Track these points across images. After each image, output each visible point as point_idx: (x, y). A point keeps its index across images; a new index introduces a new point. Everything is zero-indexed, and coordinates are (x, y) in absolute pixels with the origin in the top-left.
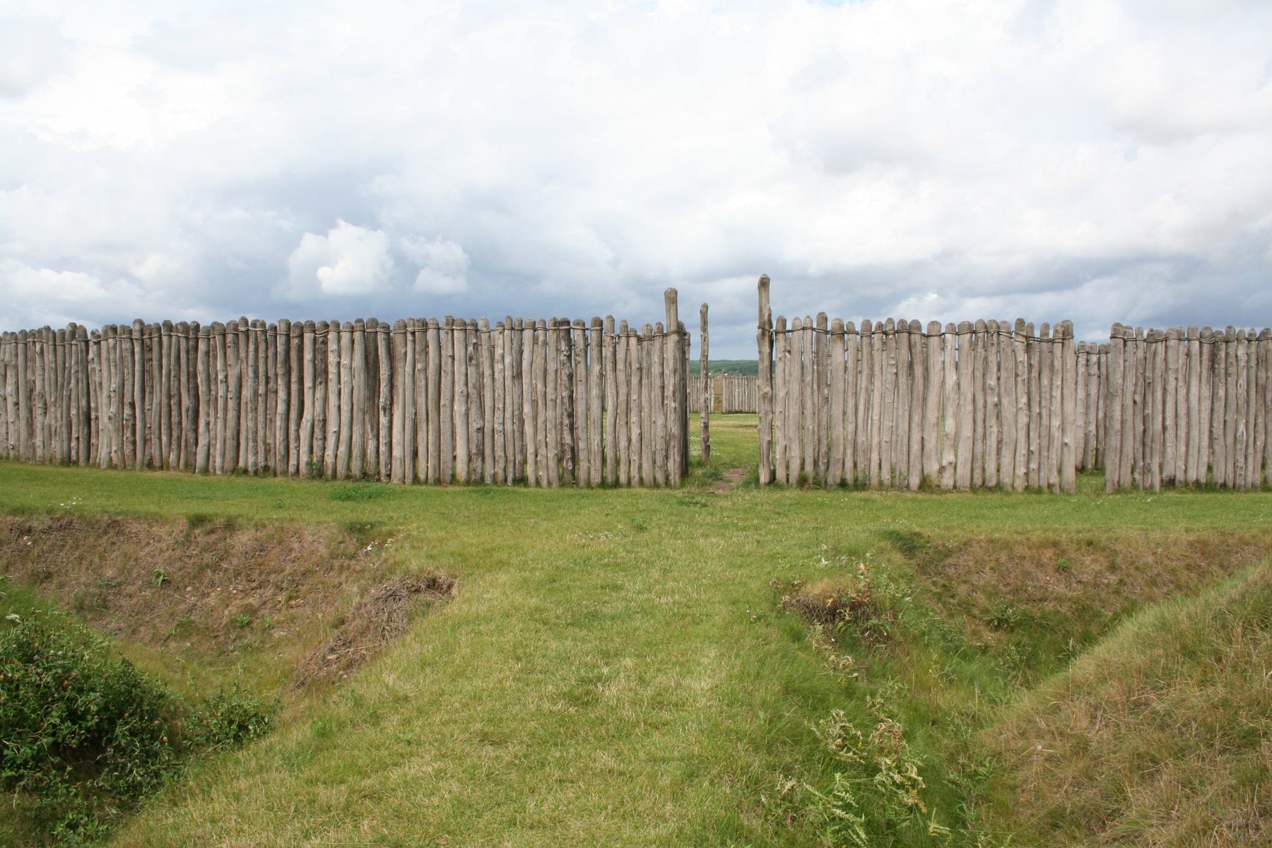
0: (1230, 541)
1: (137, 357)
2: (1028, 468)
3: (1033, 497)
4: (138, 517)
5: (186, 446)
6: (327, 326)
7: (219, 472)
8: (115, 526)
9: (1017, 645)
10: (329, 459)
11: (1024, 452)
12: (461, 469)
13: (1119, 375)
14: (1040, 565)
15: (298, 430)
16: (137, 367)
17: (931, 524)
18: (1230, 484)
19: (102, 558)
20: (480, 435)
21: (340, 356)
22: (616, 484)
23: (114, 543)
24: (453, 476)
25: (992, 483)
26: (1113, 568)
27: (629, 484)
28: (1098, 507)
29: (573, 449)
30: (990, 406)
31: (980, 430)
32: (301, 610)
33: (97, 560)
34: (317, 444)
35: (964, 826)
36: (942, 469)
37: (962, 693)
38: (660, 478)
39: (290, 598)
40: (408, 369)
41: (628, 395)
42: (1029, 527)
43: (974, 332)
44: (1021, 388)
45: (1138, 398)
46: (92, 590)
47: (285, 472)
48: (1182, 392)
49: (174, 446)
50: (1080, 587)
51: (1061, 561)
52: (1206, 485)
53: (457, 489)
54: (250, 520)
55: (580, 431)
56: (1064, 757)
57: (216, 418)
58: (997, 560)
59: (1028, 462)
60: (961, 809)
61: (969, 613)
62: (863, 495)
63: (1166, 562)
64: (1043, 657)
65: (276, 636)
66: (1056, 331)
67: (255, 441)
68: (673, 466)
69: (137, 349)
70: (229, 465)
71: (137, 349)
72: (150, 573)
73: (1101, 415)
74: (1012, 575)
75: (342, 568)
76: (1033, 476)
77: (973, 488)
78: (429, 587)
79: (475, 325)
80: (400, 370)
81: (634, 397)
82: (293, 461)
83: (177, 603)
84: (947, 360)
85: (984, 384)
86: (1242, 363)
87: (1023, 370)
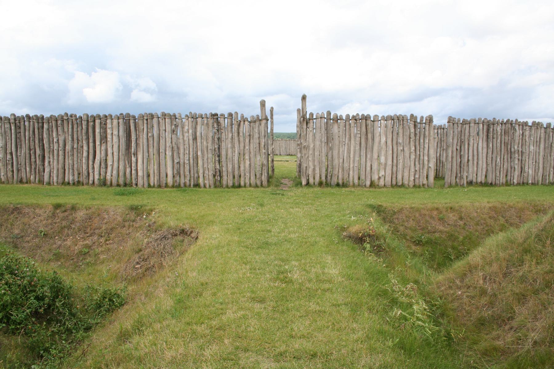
0: (506, 207)
1: (13, 131)
3: (418, 189)
4: (28, 206)
5: (39, 173)
6: (106, 116)
7: (55, 184)
8: (17, 210)
10: (108, 177)
12: (170, 180)
13: (451, 138)
14: (431, 217)
15: (93, 164)
16: (13, 136)
18: (494, 183)
19: (12, 225)
20: (178, 165)
21: (112, 131)
22: (239, 186)
23: (17, 218)
24: (166, 184)
25: (400, 184)
26: (461, 218)
27: (245, 186)
29: (220, 171)
30: (399, 151)
31: (395, 161)
32: (112, 246)
33: (9, 226)
34: (103, 171)
36: (379, 178)
38: (259, 183)
39: (106, 240)
40: (145, 136)
41: (244, 147)
44: (412, 143)
45: (458, 148)
46: (9, 240)
47: (88, 184)
49: (33, 173)
50: (448, 226)
53: (168, 189)
54: (83, 205)
55: (223, 163)
57: (53, 159)
58: (415, 216)
59: (415, 175)
61: (405, 239)
62: (347, 189)
63: (482, 215)
65: (101, 258)
66: (426, 119)
67: (73, 170)
68: (264, 178)
69: (13, 128)
70: (60, 180)
71: (13, 128)
72: (36, 231)
74: (421, 222)
75: (129, 226)
76: (417, 181)
77: (392, 186)
78: (181, 233)
79: (175, 115)
80: (141, 136)
81: (247, 147)
82: (91, 178)
83: (52, 245)
85: (397, 142)
86: (499, 133)
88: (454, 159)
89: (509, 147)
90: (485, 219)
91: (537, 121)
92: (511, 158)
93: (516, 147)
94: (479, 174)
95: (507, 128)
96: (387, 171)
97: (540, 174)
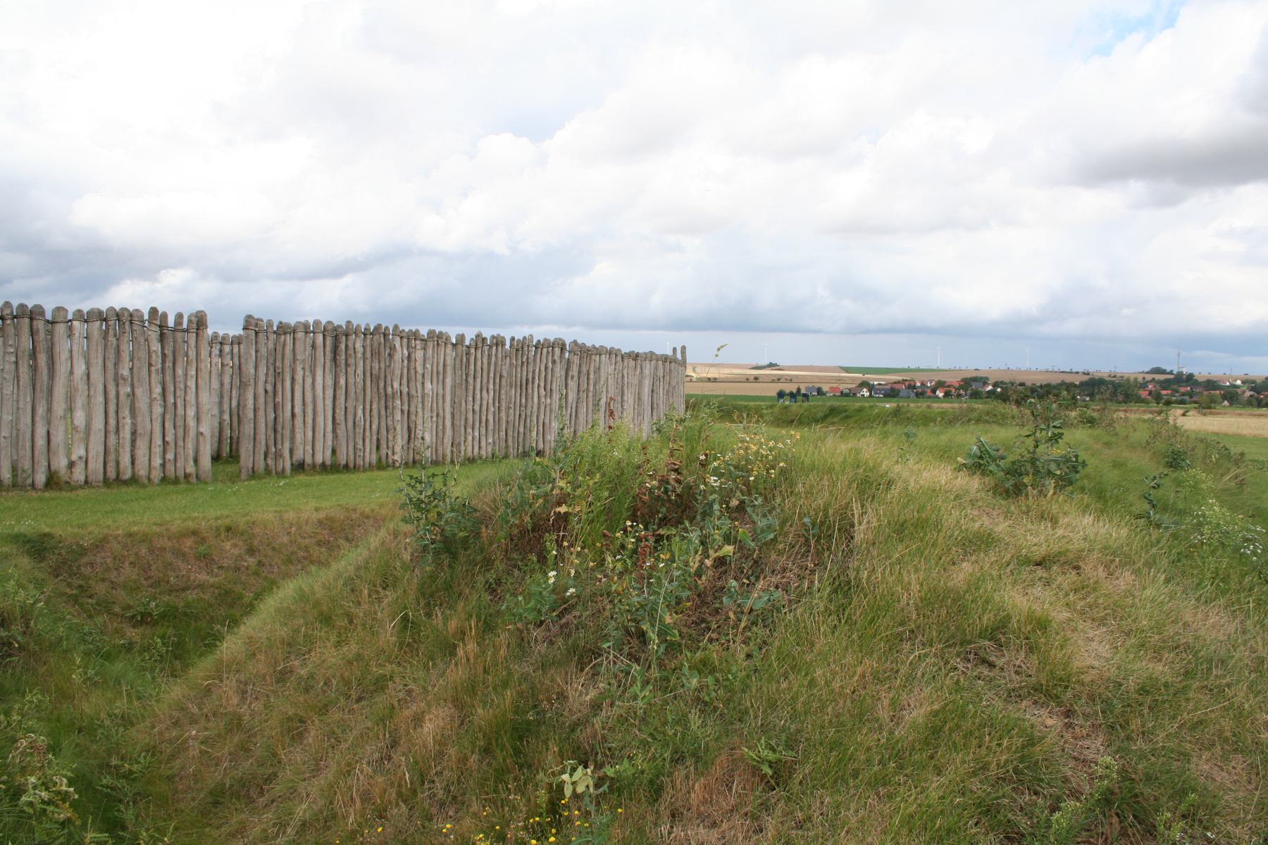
0: (354, 516)
2: (164, 459)
3: (171, 488)
9: (163, 637)
11: (160, 442)
17: (62, 521)
18: (351, 465)
25: (127, 475)
26: (251, 551)
28: (235, 493)
30: (122, 398)
31: (112, 422)
35: (124, 828)
36: (71, 465)
37: (109, 695)
42: (168, 518)
43: (105, 320)
44: (156, 378)
45: (270, 388)
48: (309, 381)
51: (202, 548)
52: (332, 466)
56: (219, 735)
60: (119, 810)
61: (109, 612)
63: (299, 540)
64: (190, 645)
66: (190, 321)
73: (234, 404)
74: (153, 568)
76: (170, 468)
77: (106, 482)
84: (75, 348)
85: (116, 374)
86: (359, 355)
87: (157, 360)
88: (261, 413)
89: (382, 385)
90: (306, 549)
91: (487, 333)
92: (386, 408)
93: (396, 385)
94: (319, 446)
95: (376, 344)
96: (91, 447)
97: (448, 441)
